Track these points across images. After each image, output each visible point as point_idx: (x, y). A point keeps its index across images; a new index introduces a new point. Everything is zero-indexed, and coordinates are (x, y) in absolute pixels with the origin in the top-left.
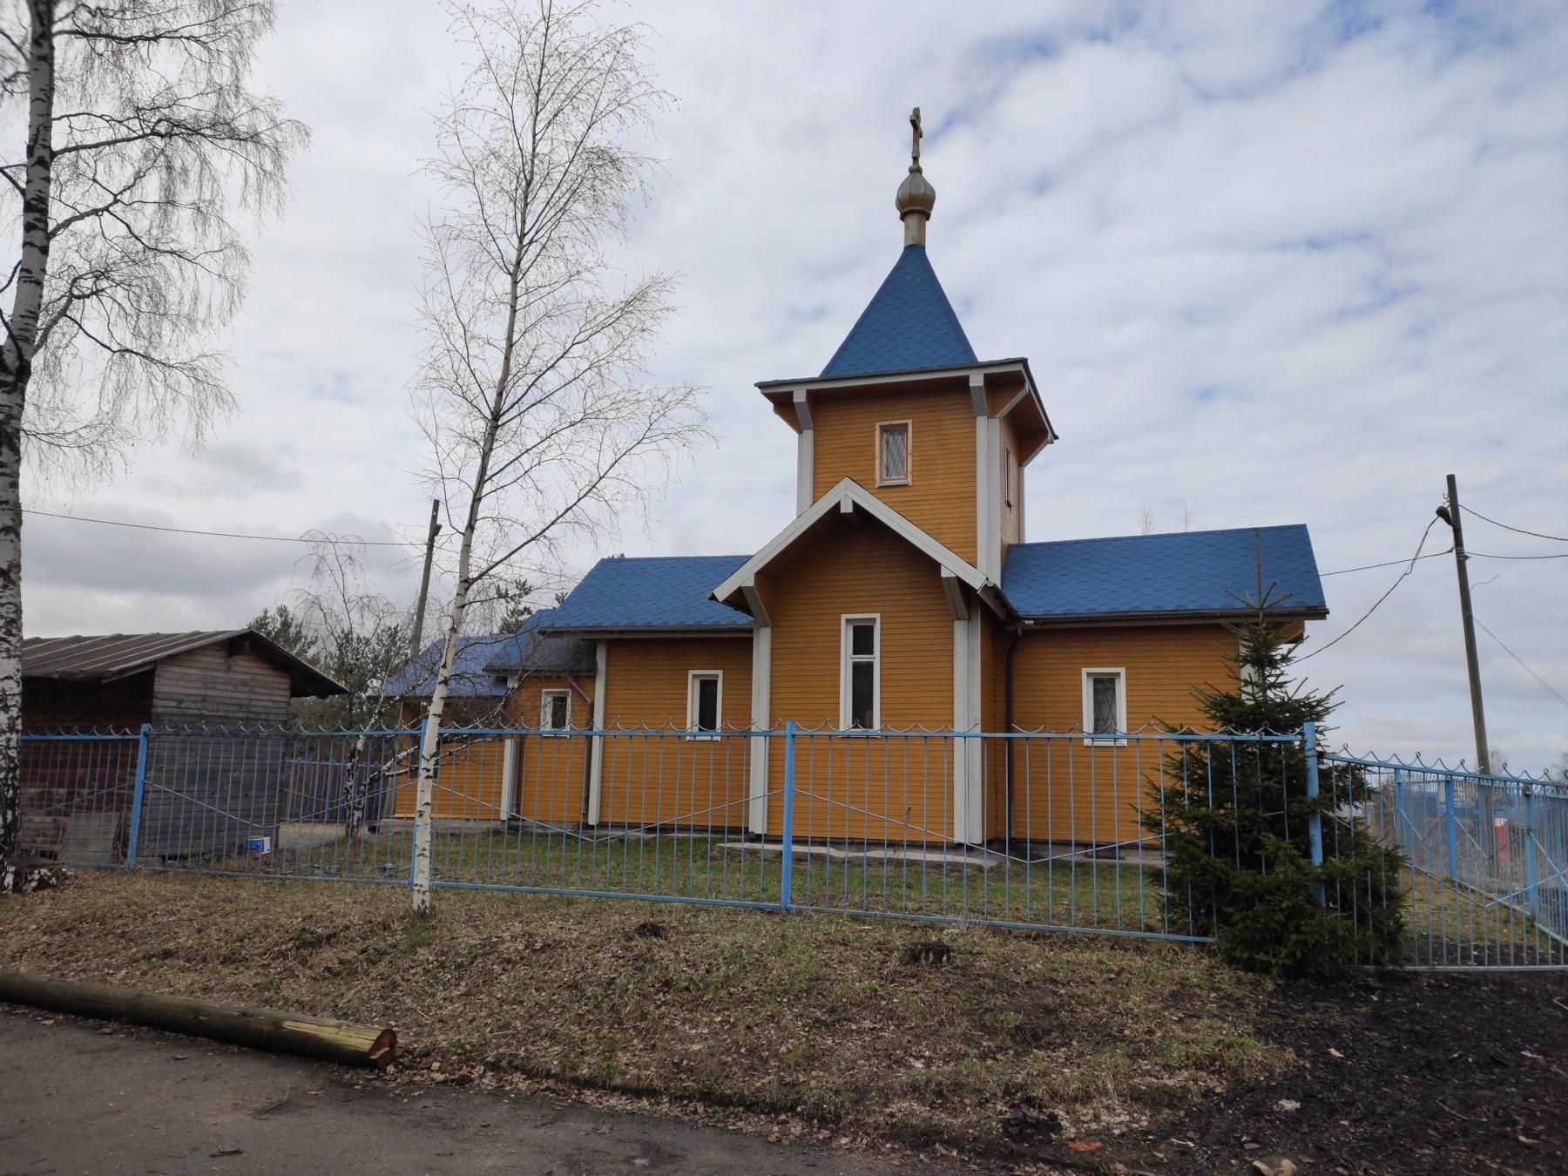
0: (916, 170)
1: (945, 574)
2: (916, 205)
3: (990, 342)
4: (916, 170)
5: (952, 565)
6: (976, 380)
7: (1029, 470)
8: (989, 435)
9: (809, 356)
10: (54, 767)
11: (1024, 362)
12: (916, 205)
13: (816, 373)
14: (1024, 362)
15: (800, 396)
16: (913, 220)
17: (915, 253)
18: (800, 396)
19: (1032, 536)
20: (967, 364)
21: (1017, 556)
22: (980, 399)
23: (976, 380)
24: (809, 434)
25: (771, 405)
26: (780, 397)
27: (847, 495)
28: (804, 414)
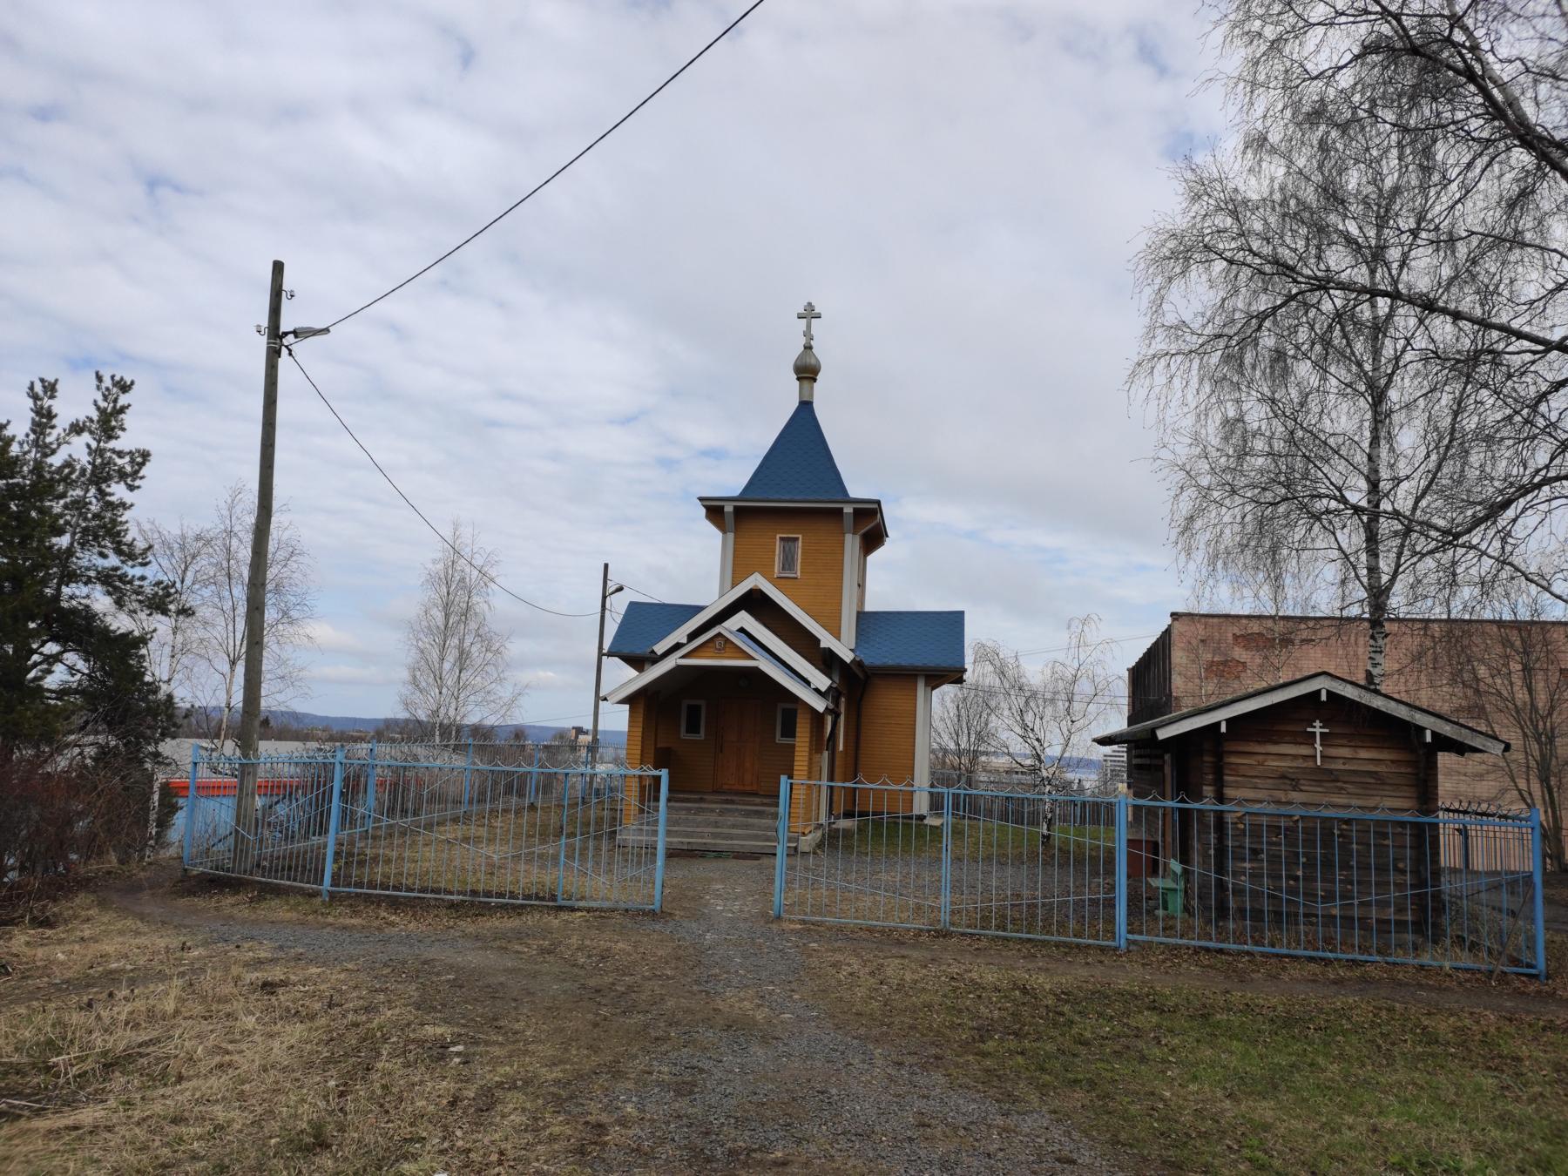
0: (808, 348)
1: (823, 645)
2: (807, 372)
3: (858, 488)
4: (808, 348)
5: (827, 640)
6: (848, 509)
7: (869, 558)
8: (852, 543)
9: (732, 481)
10: (1079, 904)
11: (878, 502)
12: (807, 372)
13: (736, 493)
14: (878, 502)
15: (729, 508)
16: (806, 384)
17: (806, 407)
18: (729, 508)
19: (868, 608)
20: (840, 498)
21: (866, 621)
22: (848, 522)
23: (848, 509)
24: (731, 536)
25: (704, 511)
26: (714, 511)
27: (756, 581)
28: (730, 520)
